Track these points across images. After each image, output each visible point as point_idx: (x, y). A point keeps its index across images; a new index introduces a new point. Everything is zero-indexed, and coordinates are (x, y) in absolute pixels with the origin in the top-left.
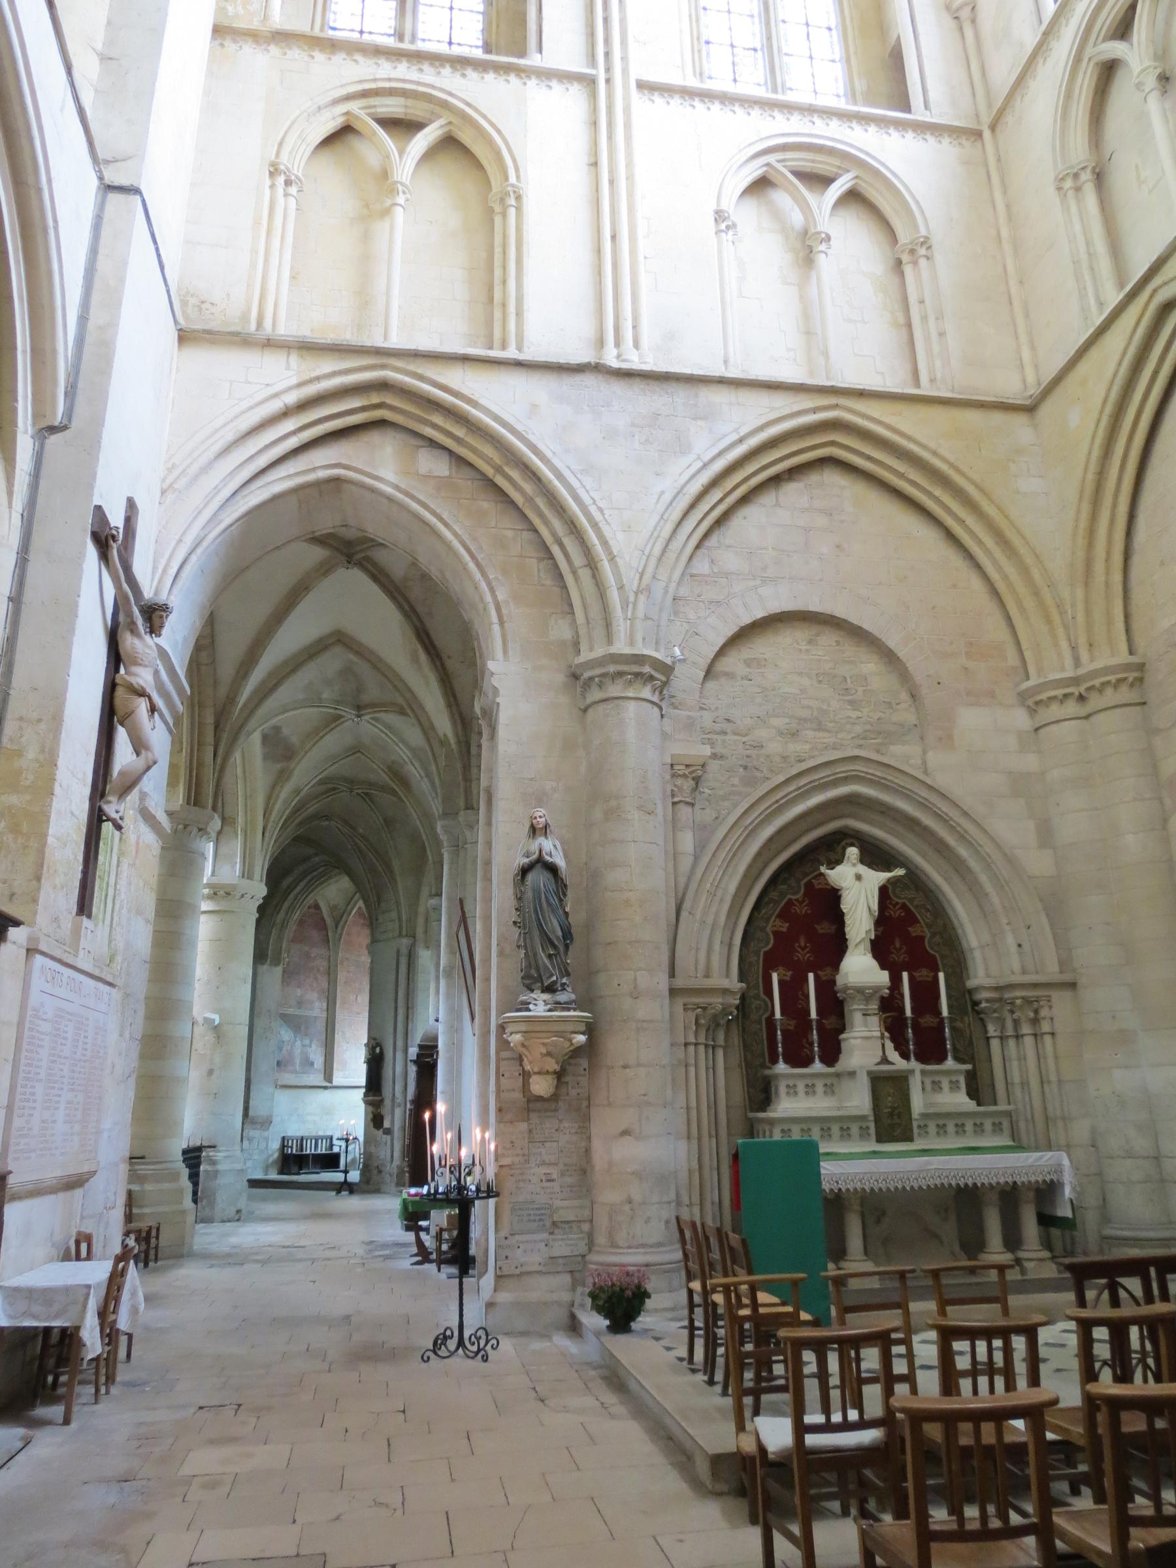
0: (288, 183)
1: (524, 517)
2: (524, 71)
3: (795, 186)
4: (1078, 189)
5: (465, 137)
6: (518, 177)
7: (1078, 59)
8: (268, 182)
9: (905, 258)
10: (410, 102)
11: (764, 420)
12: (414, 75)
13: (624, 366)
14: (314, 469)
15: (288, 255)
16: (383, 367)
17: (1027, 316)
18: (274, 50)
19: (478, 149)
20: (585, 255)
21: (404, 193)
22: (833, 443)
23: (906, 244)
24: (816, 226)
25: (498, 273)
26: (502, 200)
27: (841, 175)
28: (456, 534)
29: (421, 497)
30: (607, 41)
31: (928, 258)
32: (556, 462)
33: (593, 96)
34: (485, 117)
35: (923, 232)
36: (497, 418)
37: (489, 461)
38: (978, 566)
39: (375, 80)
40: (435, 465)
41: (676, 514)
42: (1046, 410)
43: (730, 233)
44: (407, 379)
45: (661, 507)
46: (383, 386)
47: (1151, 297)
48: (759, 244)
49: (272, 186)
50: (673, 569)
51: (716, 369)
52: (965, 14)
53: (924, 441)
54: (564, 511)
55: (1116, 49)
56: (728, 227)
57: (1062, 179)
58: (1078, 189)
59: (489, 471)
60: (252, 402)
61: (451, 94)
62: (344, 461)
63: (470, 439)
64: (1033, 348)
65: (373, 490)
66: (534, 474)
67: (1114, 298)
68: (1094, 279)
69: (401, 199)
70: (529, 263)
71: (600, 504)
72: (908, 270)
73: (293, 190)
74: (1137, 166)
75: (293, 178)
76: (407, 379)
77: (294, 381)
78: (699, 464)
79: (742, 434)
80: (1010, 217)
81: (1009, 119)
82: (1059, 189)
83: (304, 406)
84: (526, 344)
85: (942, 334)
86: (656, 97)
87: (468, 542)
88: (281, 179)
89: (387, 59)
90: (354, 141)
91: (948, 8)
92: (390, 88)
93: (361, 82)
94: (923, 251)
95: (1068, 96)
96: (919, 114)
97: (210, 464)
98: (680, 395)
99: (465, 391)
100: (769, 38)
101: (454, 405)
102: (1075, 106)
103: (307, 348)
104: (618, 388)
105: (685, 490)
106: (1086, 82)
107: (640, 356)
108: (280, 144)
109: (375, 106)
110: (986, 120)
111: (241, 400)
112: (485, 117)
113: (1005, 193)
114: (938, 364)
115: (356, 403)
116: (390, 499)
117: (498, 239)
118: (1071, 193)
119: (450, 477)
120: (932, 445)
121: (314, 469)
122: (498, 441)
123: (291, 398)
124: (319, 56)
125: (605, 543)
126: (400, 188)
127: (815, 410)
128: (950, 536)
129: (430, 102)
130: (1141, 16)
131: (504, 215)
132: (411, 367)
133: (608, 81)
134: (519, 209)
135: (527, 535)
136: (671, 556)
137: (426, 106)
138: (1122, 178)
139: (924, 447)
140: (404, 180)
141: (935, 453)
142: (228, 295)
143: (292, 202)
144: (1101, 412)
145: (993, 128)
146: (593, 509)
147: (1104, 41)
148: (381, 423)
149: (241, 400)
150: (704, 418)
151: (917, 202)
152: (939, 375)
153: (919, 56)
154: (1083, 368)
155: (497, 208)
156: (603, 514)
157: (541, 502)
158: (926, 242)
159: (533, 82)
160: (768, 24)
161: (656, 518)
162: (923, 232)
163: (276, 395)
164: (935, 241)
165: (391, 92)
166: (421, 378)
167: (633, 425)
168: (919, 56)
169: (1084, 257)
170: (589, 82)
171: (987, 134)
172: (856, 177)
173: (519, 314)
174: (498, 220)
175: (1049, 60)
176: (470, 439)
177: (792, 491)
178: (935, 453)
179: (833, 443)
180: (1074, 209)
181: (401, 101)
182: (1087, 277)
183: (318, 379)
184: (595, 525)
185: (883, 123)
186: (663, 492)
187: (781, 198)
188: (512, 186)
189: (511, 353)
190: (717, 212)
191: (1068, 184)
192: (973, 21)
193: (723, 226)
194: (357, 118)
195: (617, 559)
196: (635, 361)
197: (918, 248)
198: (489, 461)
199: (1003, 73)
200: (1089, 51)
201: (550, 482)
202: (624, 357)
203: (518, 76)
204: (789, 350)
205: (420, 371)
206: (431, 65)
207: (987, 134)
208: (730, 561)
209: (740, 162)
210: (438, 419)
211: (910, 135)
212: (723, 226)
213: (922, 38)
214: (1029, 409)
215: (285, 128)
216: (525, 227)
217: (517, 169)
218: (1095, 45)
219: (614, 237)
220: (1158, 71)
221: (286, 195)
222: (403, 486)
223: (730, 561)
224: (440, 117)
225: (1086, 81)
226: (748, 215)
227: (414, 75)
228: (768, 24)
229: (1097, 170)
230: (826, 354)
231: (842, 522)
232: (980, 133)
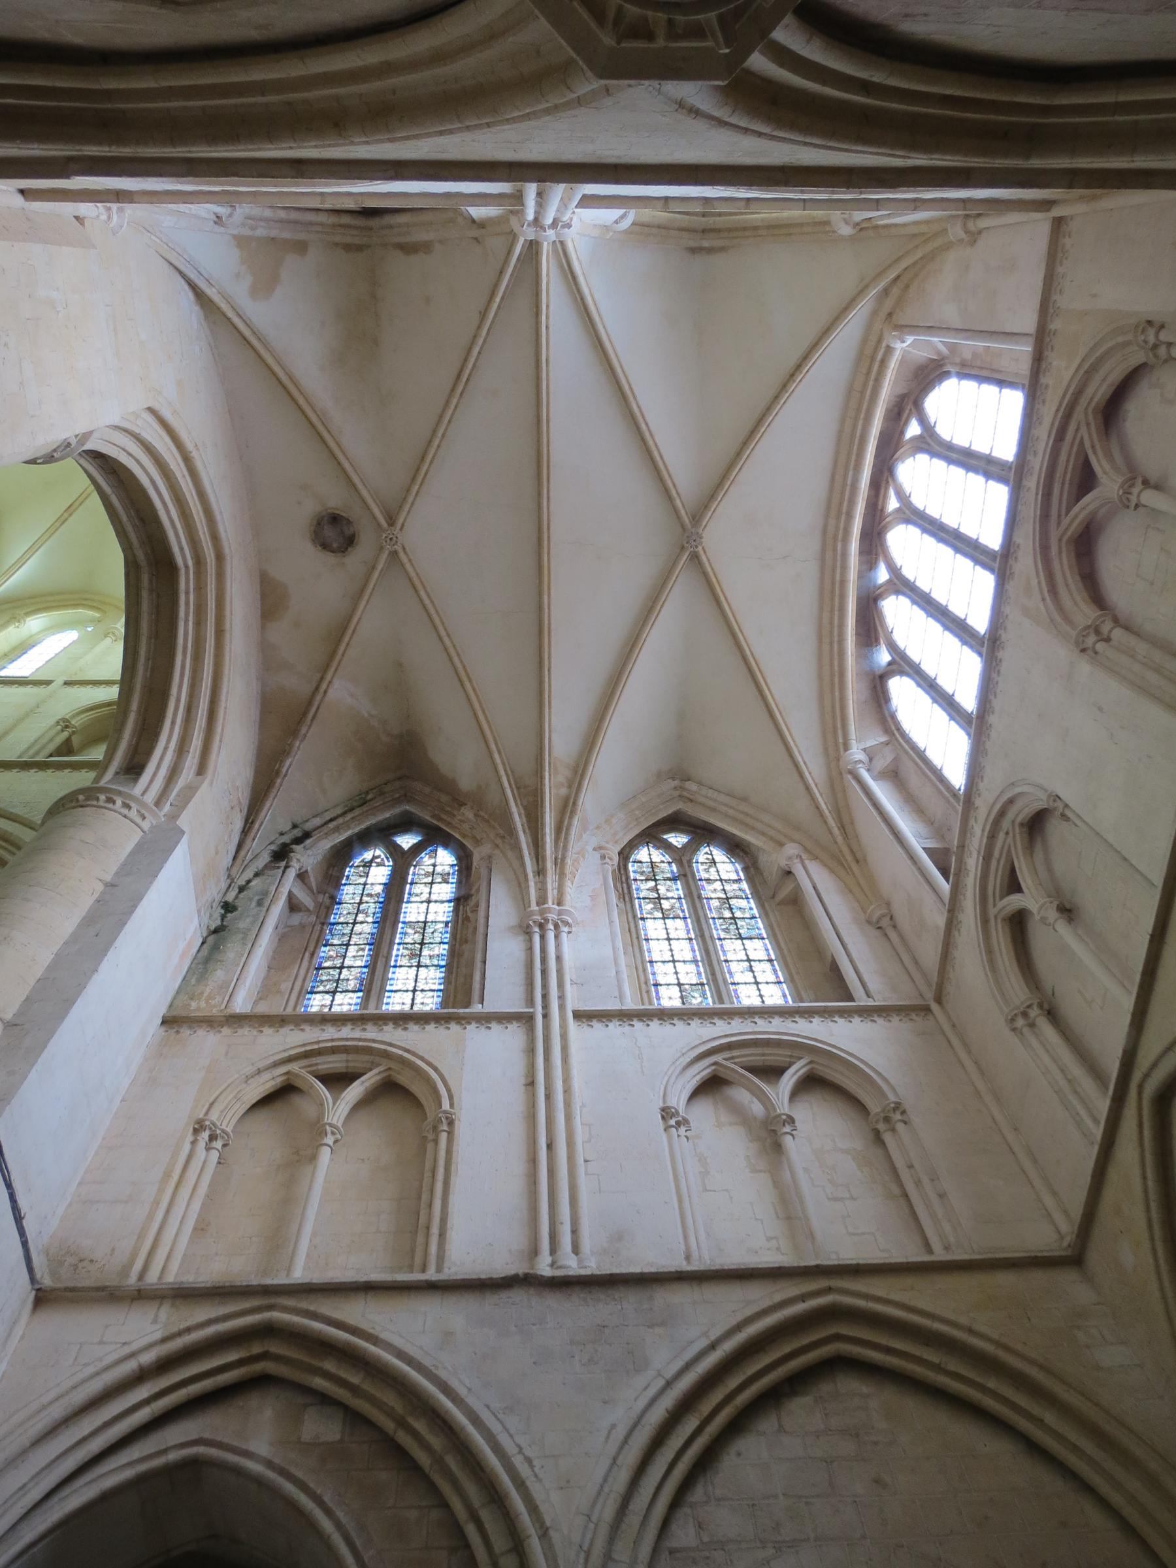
0: (213, 1138)
1: (433, 1488)
2: (464, 1018)
3: (748, 1079)
4: (1032, 1025)
5: (403, 1079)
6: (452, 1105)
7: (985, 921)
8: (190, 1138)
9: (881, 1126)
10: (350, 1057)
11: (739, 1317)
12: (357, 1034)
13: (559, 1273)
14: (165, 1451)
15: (196, 1206)
16: (270, 1308)
17: (1035, 1161)
18: (226, 1031)
19: (416, 1088)
20: (519, 1167)
21: (333, 1133)
22: (838, 1337)
23: (877, 1114)
24: (775, 1110)
25: (425, 1197)
26: (435, 1128)
27: (794, 1063)
28: (338, 1525)
29: (299, 1474)
30: (545, 986)
31: (905, 1123)
32: (471, 1401)
33: (531, 1030)
34: (422, 1059)
35: (892, 1098)
36: (401, 1354)
37: (390, 1413)
38: (1088, 1489)
39: (319, 1042)
40: (321, 1428)
41: (632, 1456)
42: (1093, 1257)
43: (682, 1129)
44: (296, 1319)
45: (612, 1448)
46: (268, 1331)
47: (1140, 1093)
48: (717, 1137)
49: (194, 1143)
50: (636, 1543)
51: (674, 1262)
52: (885, 922)
53: (952, 1317)
54: (482, 1469)
55: (1014, 902)
56: (678, 1124)
57: (1013, 1020)
58: (1032, 1025)
59: (389, 1425)
60: (100, 1365)
61: (391, 1045)
62: (207, 1435)
63: (368, 1387)
64: (1054, 1193)
65: (237, 1471)
66: (445, 1422)
67: (1103, 1106)
68: (1082, 1101)
69: (329, 1140)
70: (457, 1183)
71: (528, 1452)
72: (888, 1137)
73: (218, 1144)
74: (1079, 991)
75: (218, 1132)
76: (296, 1319)
77: (158, 1335)
78: (661, 1383)
79: (713, 1338)
80: (982, 1072)
81: (950, 989)
82: (1014, 1030)
83: (164, 1365)
84: (446, 1265)
85: (942, 1196)
86: (594, 1023)
87: (353, 1534)
88: (205, 1135)
89: (333, 1025)
90: (296, 1100)
91: (869, 922)
92: (332, 1047)
93: (304, 1045)
94: (898, 1116)
95: (990, 952)
96: (862, 1000)
97: (23, 1453)
98: (629, 1302)
99: (364, 1326)
100: (713, 974)
101: (348, 1344)
102: (1000, 962)
103: (184, 1295)
104: (553, 1302)
105: (643, 1422)
106: (1001, 939)
107: (580, 1261)
108: (212, 1104)
109: (316, 1064)
110: (929, 995)
111: (86, 1365)
112: (422, 1059)
113: (969, 1052)
114: (947, 1228)
115: (232, 1356)
116: (259, 1482)
117: (428, 1165)
118: (1026, 1030)
119: (341, 1441)
120: (963, 1320)
121: (165, 1451)
122: (403, 1384)
123: (147, 1358)
124: (268, 1031)
125: (533, 1509)
126: (328, 1128)
127: (803, 1298)
128: (1033, 1448)
129: (371, 1054)
130: (1020, 868)
131: (436, 1141)
132: (304, 1305)
133: (545, 1016)
134: (450, 1133)
135: (436, 1514)
136: (633, 1519)
137: (367, 1058)
138: (1071, 1006)
139: (955, 1325)
140: (334, 1122)
141: (970, 1331)
142: (113, 1250)
143: (214, 1156)
144: (1152, 1239)
145: (939, 1000)
146: (518, 1461)
147: (1002, 898)
148: (261, 1382)
149: (86, 1365)
150: (663, 1324)
151: (879, 1074)
152: (952, 1240)
153: (852, 961)
154: (1109, 1195)
155: (431, 1136)
156: (531, 1466)
157: (452, 1462)
158: (897, 1107)
159: (472, 1027)
160: (711, 965)
161: (605, 1463)
162: (892, 1098)
163: (132, 1355)
164: (907, 1104)
165: (334, 1050)
166: (314, 1316)
167: (572, 1343)
168: (852, 961)
169: (1063, 1083)
170: (527, 1020)
171: (935, 1007)
172: (811, 1062)
173: (442, 1235)
174: (430, 1146)
175: (962, 930)
176: (368, 1387)
177: (800, 1411)
178: (970, 1331)
179: (838, 1337)
180: (1034, 1042)
181: (343, 1057)
182: (1075, 1102)
183: (188, 1330)
184: (521, 1485)
185: (826, 1013)
186: (613, 1426)
187: (740, 1095)
188: (445, 1112)
189: (431, 1275)
190: (663, 1110)
191: (1020, 1022)
192: (895, 927)
193: (672, 1122)
194: (297, 1075)
195: (552, 1533)
196: (572, 1266)
197: (892, 1115)
198: (390, 1413)
199: (930, 954)
200: (992, 911)
201: (463, 1428)
202: (559, 1264)
203: (458, 1023)
204: (769, 1239)
205: (312, 1308)
206: (375, 1024)
207: (935, 1007)
208: (726, 1521)
209: (684, 1064)
210: (329, 1365)
211: (856, 1020)
212: (672, 1122)
213: (850, 947)
214: (1075, 1259)
215: (218, 1093)
216: (455, 1149)
217: (451, 1098)
218: (995, 905)
219: (550, 1146)
220: (1056, 903)
221: (208, 1149)
222: (277, 1461)
223: (726, 1521)
224: (379, 1065)
225: (1001, 939)
226: (704, 1115)
227: (357, 1034)
228: (711, 965)
229: (1046, 1006)
230: (812, 1236)
231: (876, 1443)
232: (926, 1004)
